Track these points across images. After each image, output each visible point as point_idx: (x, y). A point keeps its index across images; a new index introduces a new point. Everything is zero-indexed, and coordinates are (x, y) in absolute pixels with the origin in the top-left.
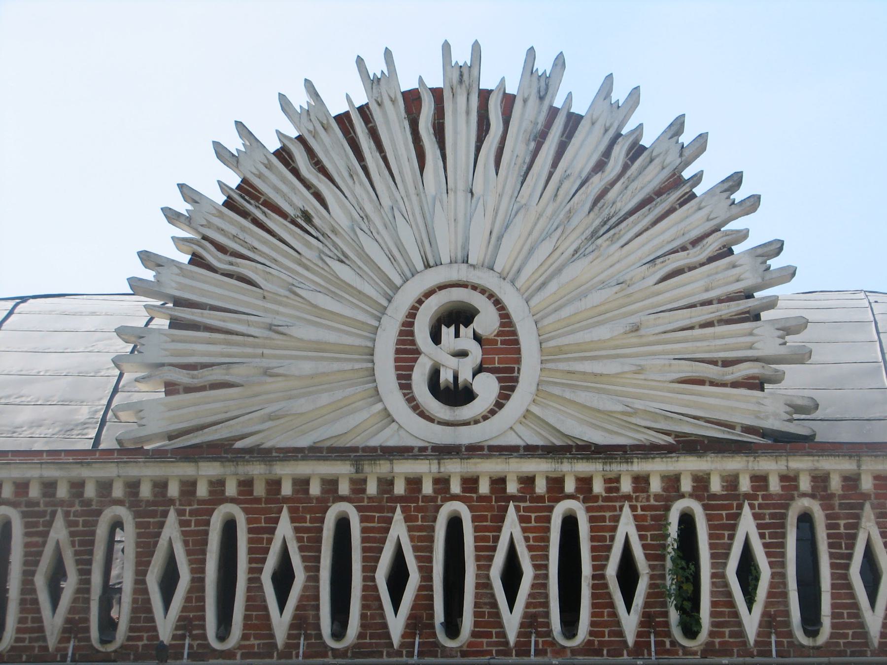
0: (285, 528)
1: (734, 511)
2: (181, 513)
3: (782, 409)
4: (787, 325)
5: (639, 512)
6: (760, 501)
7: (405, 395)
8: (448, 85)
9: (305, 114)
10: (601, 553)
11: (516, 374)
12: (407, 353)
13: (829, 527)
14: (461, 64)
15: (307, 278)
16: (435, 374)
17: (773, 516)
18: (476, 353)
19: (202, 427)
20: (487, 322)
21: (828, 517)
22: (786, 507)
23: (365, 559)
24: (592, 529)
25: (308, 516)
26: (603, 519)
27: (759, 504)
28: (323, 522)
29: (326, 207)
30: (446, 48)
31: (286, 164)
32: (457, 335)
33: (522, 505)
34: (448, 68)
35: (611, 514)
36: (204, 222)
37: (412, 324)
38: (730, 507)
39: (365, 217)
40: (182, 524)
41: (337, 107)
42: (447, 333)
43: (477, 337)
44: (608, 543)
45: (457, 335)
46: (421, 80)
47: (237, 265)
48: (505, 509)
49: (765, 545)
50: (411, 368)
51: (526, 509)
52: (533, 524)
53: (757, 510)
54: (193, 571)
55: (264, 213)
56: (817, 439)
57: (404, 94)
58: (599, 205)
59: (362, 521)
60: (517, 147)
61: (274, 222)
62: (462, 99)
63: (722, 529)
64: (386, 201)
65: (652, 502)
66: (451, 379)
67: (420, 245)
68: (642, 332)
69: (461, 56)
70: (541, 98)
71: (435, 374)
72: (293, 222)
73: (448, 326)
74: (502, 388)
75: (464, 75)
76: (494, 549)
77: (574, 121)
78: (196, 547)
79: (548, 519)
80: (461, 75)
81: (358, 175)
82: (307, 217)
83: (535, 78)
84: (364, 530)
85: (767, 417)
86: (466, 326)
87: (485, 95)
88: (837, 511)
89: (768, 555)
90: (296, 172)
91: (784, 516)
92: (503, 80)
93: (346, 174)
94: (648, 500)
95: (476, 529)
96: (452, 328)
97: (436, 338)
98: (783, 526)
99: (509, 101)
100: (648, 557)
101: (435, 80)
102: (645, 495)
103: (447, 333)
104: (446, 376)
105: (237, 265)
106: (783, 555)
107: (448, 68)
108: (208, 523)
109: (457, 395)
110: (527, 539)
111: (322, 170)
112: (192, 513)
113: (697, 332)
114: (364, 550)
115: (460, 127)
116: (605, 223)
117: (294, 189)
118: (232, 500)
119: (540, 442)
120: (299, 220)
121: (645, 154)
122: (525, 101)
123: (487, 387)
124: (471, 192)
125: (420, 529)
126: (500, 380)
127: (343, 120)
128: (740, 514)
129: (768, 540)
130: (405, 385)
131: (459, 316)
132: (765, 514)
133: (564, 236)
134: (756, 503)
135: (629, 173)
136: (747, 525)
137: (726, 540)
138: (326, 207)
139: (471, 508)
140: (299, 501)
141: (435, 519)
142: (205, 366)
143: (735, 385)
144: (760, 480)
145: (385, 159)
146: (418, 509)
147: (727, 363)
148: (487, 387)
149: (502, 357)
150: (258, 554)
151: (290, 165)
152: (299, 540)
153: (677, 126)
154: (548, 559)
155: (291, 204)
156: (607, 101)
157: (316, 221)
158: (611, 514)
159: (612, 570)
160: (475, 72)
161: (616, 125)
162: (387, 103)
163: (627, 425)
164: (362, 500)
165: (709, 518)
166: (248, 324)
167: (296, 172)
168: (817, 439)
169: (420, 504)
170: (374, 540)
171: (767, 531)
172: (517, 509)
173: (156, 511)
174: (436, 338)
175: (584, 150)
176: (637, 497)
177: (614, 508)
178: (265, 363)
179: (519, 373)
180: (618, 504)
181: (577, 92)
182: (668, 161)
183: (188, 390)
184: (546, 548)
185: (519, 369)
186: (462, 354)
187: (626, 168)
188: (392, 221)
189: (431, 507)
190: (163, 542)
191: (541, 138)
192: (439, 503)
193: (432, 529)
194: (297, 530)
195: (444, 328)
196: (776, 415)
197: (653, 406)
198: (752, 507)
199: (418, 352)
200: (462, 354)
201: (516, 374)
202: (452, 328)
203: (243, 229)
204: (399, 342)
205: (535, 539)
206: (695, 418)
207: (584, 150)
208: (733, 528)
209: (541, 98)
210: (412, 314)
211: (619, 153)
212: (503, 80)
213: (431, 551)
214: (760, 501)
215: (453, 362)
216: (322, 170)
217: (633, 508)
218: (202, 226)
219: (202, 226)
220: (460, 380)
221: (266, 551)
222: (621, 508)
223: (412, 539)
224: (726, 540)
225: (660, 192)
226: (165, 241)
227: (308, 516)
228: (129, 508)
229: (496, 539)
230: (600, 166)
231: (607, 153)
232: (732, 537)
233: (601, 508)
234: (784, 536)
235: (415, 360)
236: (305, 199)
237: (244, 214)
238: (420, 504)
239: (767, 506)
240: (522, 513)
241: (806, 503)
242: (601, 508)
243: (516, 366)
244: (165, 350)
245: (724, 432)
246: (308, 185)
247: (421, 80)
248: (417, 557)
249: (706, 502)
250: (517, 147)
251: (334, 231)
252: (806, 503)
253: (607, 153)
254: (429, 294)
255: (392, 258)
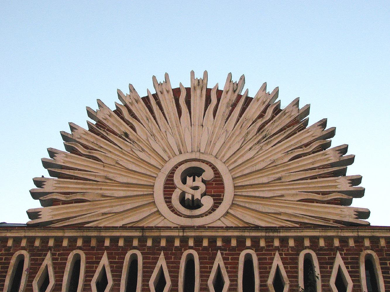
0: (105, 261)
1: (332, 256)
2: (53, 254)
3: (353, 213)
4: (353, 178)
5: (284, 256)
6: (345, 251)
7: (168, 205)
8: (193, 86)
9: (128, 97)
10: (264, 276)
11: (222, 197)
12: (169, 187)
13: (381, 264)
14: (199, 79)
15: (124, 158)
16: (183, 194)
17: (351, 259)
18: (203, 187)
19: (69, 218)
20: (208, 175)
21: (380, 259)
22: (359, 254)
23: (144, 276)
24: (260, 264)
25: (117, 257)
26: (266, 259)
27: (344, 253)
28: (124, 259)
29: (135, 132)
30: (192, 73)
31: (119, 115)
32: (194, 180)
33: (224, 252)
34: (193, 80)
35: (269, 257)
36: (79, 137)
37: (174, 173)
38: (330, 254)
39: (153, 135)
40: (53, 259)
41: (142, 94)
42: (189, 180)
43: (203, 181)
44: (268, 270)
45: (194, 180)
46: (181, 84)
47: (92, 153)
48: (216, 254)
49: (349, 272)
50: (172, 194)
51: (226, 254)
52: (230, 261)
53: (343, 256)
54: (56, 281)
55: (107, 134)
56: (371, 225)
57: (173, 90)
58: (261, 131)
59: (143, 259)
60: (223, 108)
61: (111, 137)
62: (198, 91)
63: (327, 264)
64: (163, 130)
65: (290, 252)
66: (190, 198)
67: (178, 146)
68: (283, 180)
69: (199, 76)
70: (234, 91)
71: (183, 194)
72: (120, 137)
73: (190, 177)
74: (215, 203)
75: (201, 83)
76: (210, 272)
77: (249, 100)
78: (59, 269)
79: (238, 259)
80: (199, 82)
81: (150, 119)
82: (126, 135)
83: (232, 85)
84: (144, 263)
85: (345, 217)
86: (198, 177)
87: (209, 91)
88: (385, 256)
89: (351, 276)
90: (123, 118)
91: (358, 259)
92: (217, 85)
93: (145, 119)
94: (288, 251)
95: (201, 263)
96: (192, 178)
97: (184, 182)
98: (358, 263)
99: (219, 93)
100: (289, 277)
101: (187, 84)
102: (286, 248)
103: (189, 180)
104: (188, 196)
105: (92, 153)
106: (359, 276)
107: (193, 80)
108: (66, 259)
109: (194, 205)
110: (227, 268)
111: (135, 117)
112: (59, 255)
113: (309, 181)
114: (144, 272)
115: (198, 102)
116: (264, 138)
117: (121, 124)
118: (80, 248)
119: (234, 226)
120: (123, 136)
121: (282, 112)
122: (227, 92)
123: (208, 202)
124: (202, 126)
125: (172, 263)
126: (214, 200)
127: (146, 100)
128: (335, 258)
129: (350, 270)
130: (168, 200)
131: (195, 172)
132: (348, 258)
133: (245, 142)
134: (343, 252)
135: (274, 119)
136: (339, 261)
137: (328, 269)
138: (135, 132)
139: (199, 254)
140: (114, 250)
141: (180, 259)
142: (72, 193)
143: (329, 202)
144: (344, 241)
145: (163, 114)
146: (172, 254)
147: (324, 193)
148: (208, 202)
149: (215, 189)
150: (89, 273)
151: (120, 115)
152: (111, 267)
153: (296, 102)
154: (237, 277)
155: (120, 130)
156: (264, 92)
157: (130, 136)
158: (269, 257)
159: (270, 281)
160: (205, 81)
161: (268, 101)
162: (165, 92)
163: (276, 219)
164: (144, 250)
165: (319, 259)
166: (95, 176)
167: (123, 118)
168: (371, 225)
169: (173, 251)
170: (149, 267)
171: (349, 266)
172: (222, 254)
173: (42, 254)
174: (184, 182)
175: (253, 110)
176: (282, 249)
177: (271, 254)
178: (101, 192)
179: (223, 197)
180: (273, 253)
181: (252, 89)
182: (293, 114)
183: (64, 203)
184: (237, 272)
185: (223, 195)
186: (196, 188)
187: (273, 117)
188: (166, 136)
189: (179, 250)
190: (43, 267)
191: (234, 106)
192: (183, 251)
193: (179, 263)
194: (110, 263)
195: (188, 178)
196: (349, 216)
197: (290, 211)
198: (341, 254)
199: (175, 188)
200: (196, 188)
201: (222, 197)
202: (192, 178)
203: (97, 139)
204: (166, 184)
205: (231, 268)
206: (310, 216)
207: (253, 110)
208: (332, 264)
209: (234, 91)
210: (176, 167)
211: (270, 111)
212: (217, 85)
213: (178, 273)
214: (345, 251)
215: (192, 191)
216: (135, 117)
217: (281, 254)
218: (78, 138)
219: (78, 138)
220: (195, 198)
221: (94, 272)
222: (274, 254)
223: (168, 267)
224: (328, 269)
225: (288, 126)
226: (83, 122)
227: (117, 257)
228: (29, 252)
229: (211, 268)
230: (261, 116)
231: (264, 111)
232: (331, 268)
233: (264, 254)
234: (358, 267)
235: (173, 191)
236: (126, 128)
237: (98, 134)
238: (173, 251)
239: (350, 254)
240: (224, 256)
241: (369, 252)
242: (264, 254)
243: (222, 194)
244: (55, 187)
245: (324, 222)
246: (127, 122)
247: (181, 84)
248: (170, 276)
249: (318, 252)
250: (223, 108)
251: (138, 140)
252: (369, 252)
253: (264, 111)
254: (180, 164)
255: (165, 151)
